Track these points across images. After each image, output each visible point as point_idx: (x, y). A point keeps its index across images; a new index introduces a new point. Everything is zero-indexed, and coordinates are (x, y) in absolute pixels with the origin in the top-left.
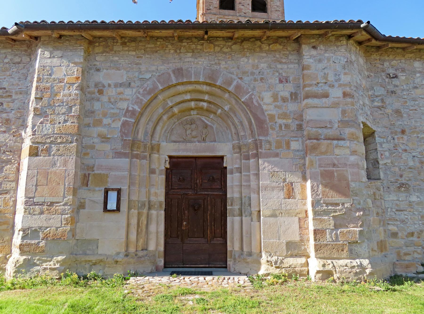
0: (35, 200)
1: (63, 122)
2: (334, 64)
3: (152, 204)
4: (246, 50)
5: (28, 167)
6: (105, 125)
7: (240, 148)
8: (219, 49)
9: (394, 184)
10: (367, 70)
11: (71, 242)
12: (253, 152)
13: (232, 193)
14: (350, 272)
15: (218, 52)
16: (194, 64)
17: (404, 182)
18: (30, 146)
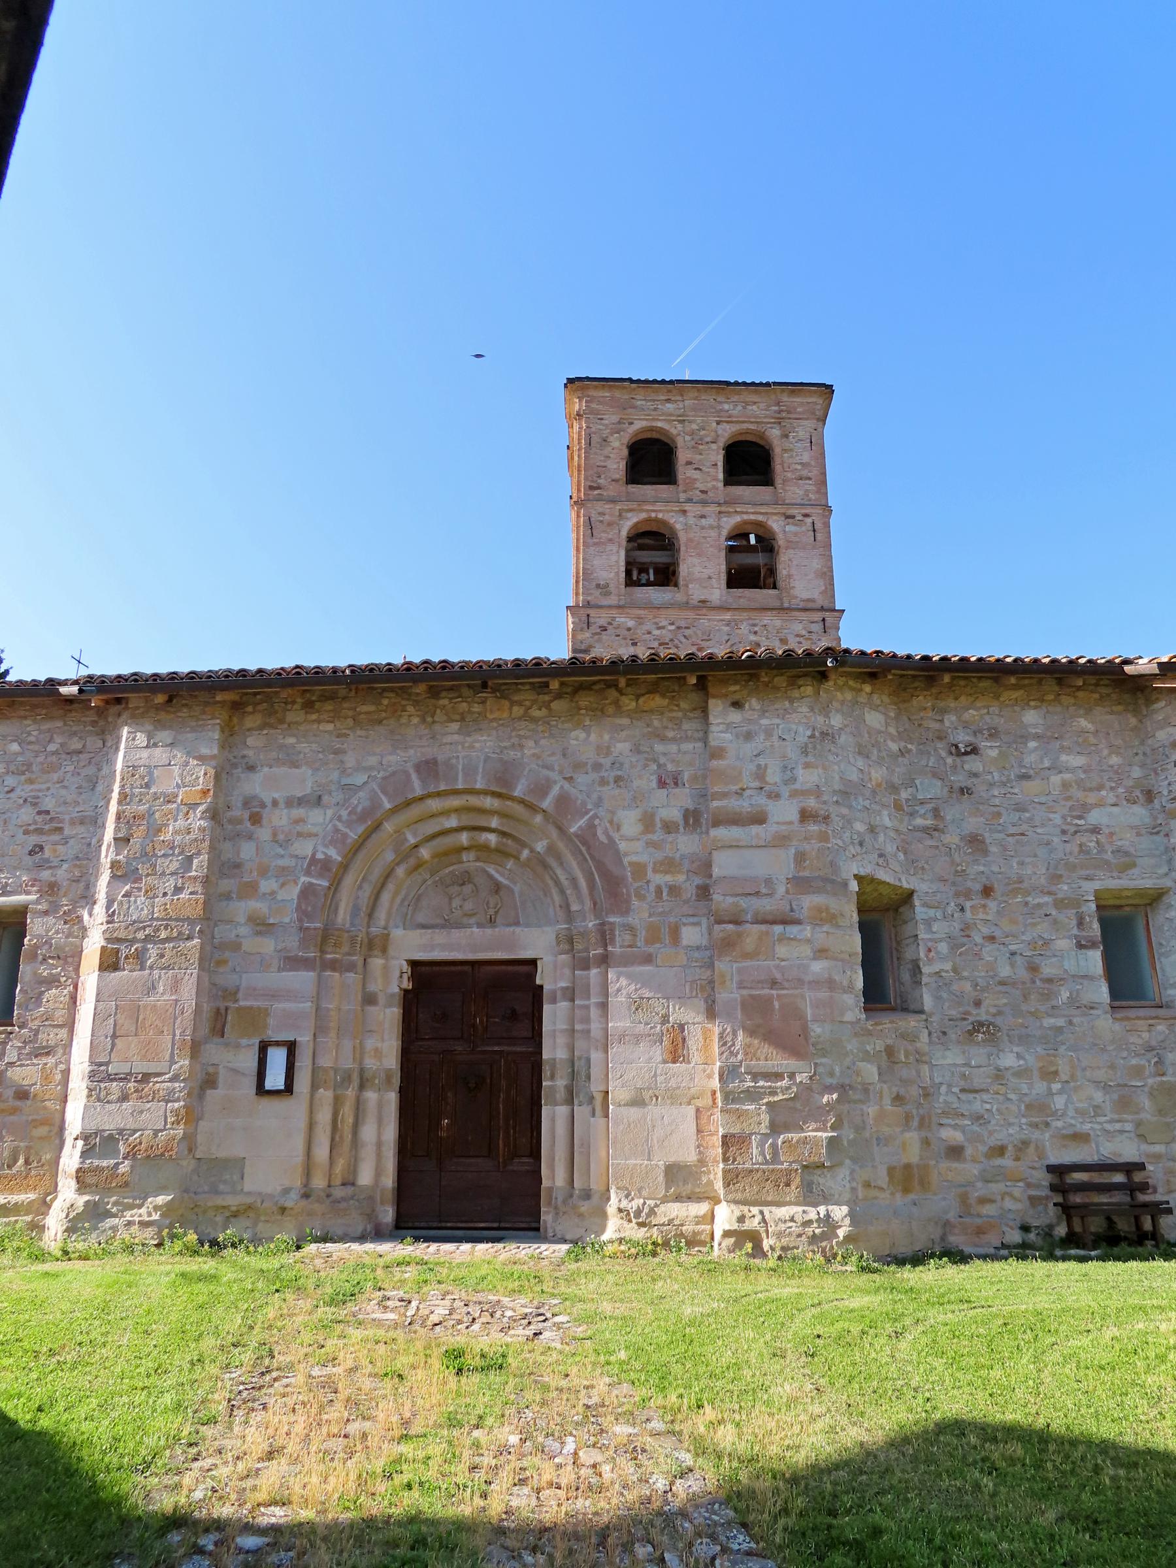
0: (111, 1069)
1: (175, 893)
2: (781, 743)
3: (367, 1075)
4: (583, 712)
5: (98, 995)
6: (264, 894)
7: (570, 940)
8: (522, 711)
9: (958, 1023)
10: (901, 736)
11: (184, 1163)
12: (594, 952)
13: (553, 1050)
14: (800, 1236)
15: (520, 719)
16: (463, 747)
17: (984, 1018)
18: (103, 947)
